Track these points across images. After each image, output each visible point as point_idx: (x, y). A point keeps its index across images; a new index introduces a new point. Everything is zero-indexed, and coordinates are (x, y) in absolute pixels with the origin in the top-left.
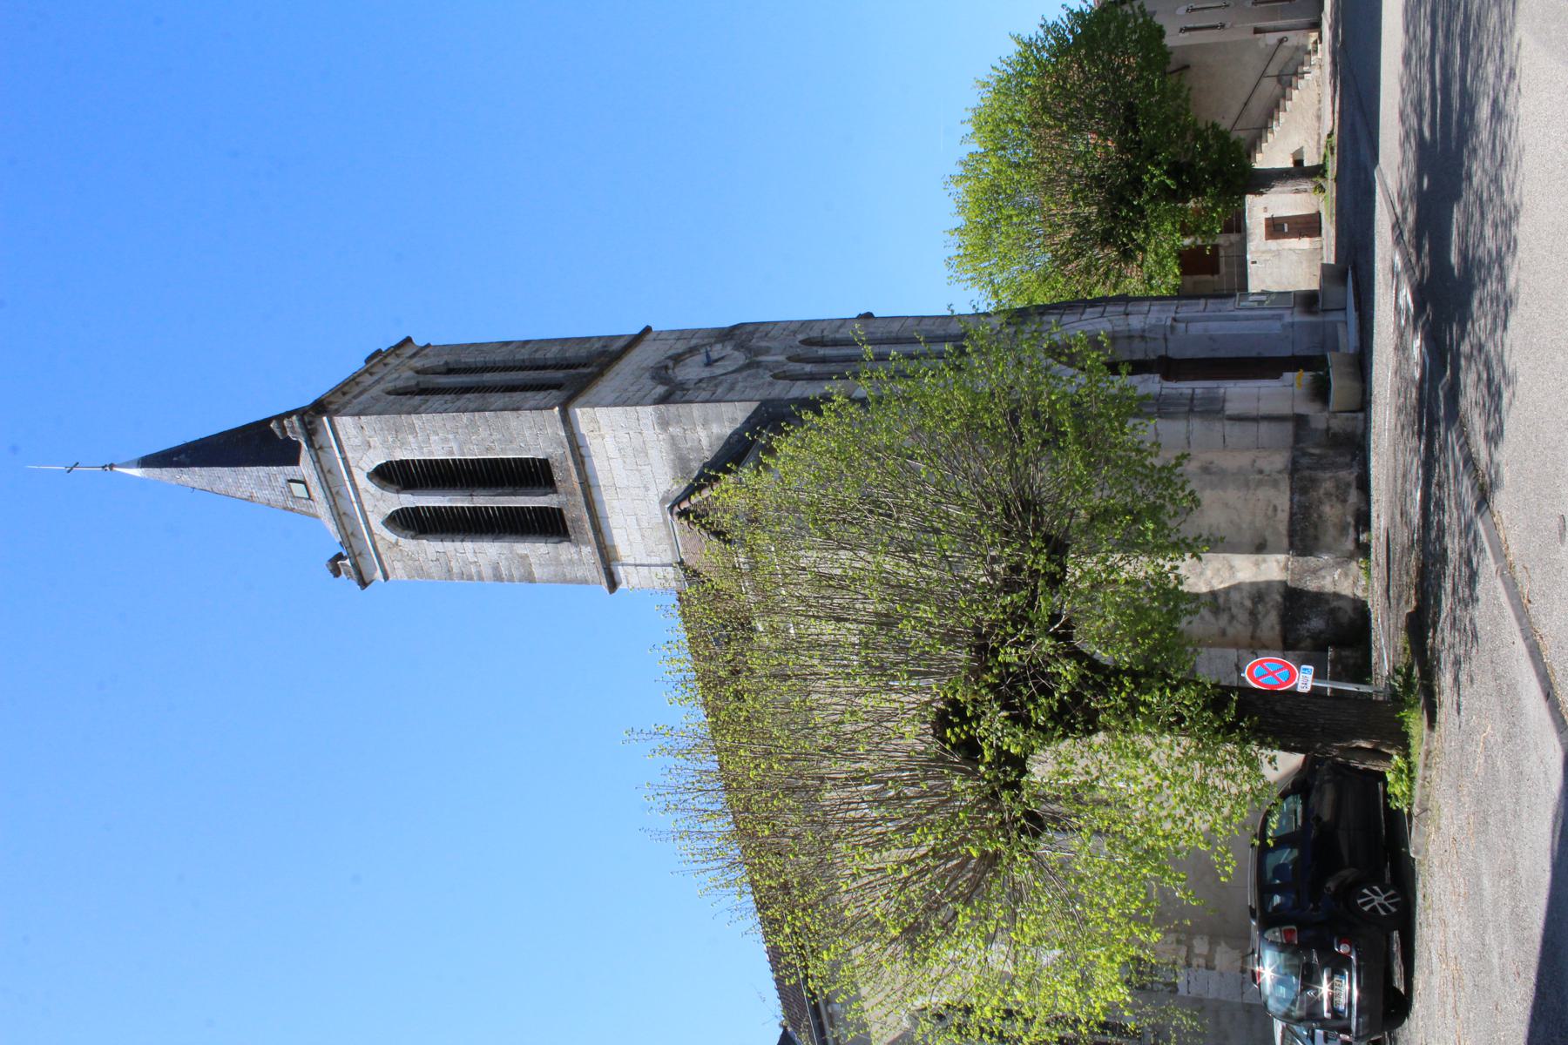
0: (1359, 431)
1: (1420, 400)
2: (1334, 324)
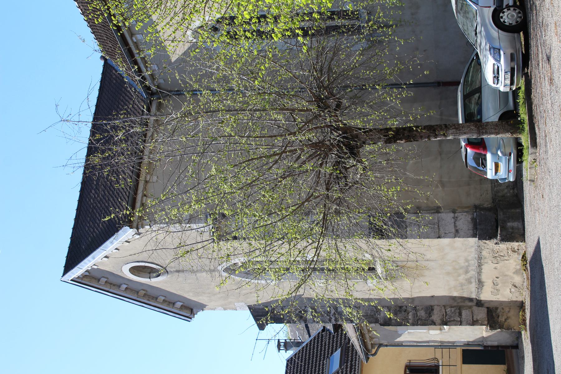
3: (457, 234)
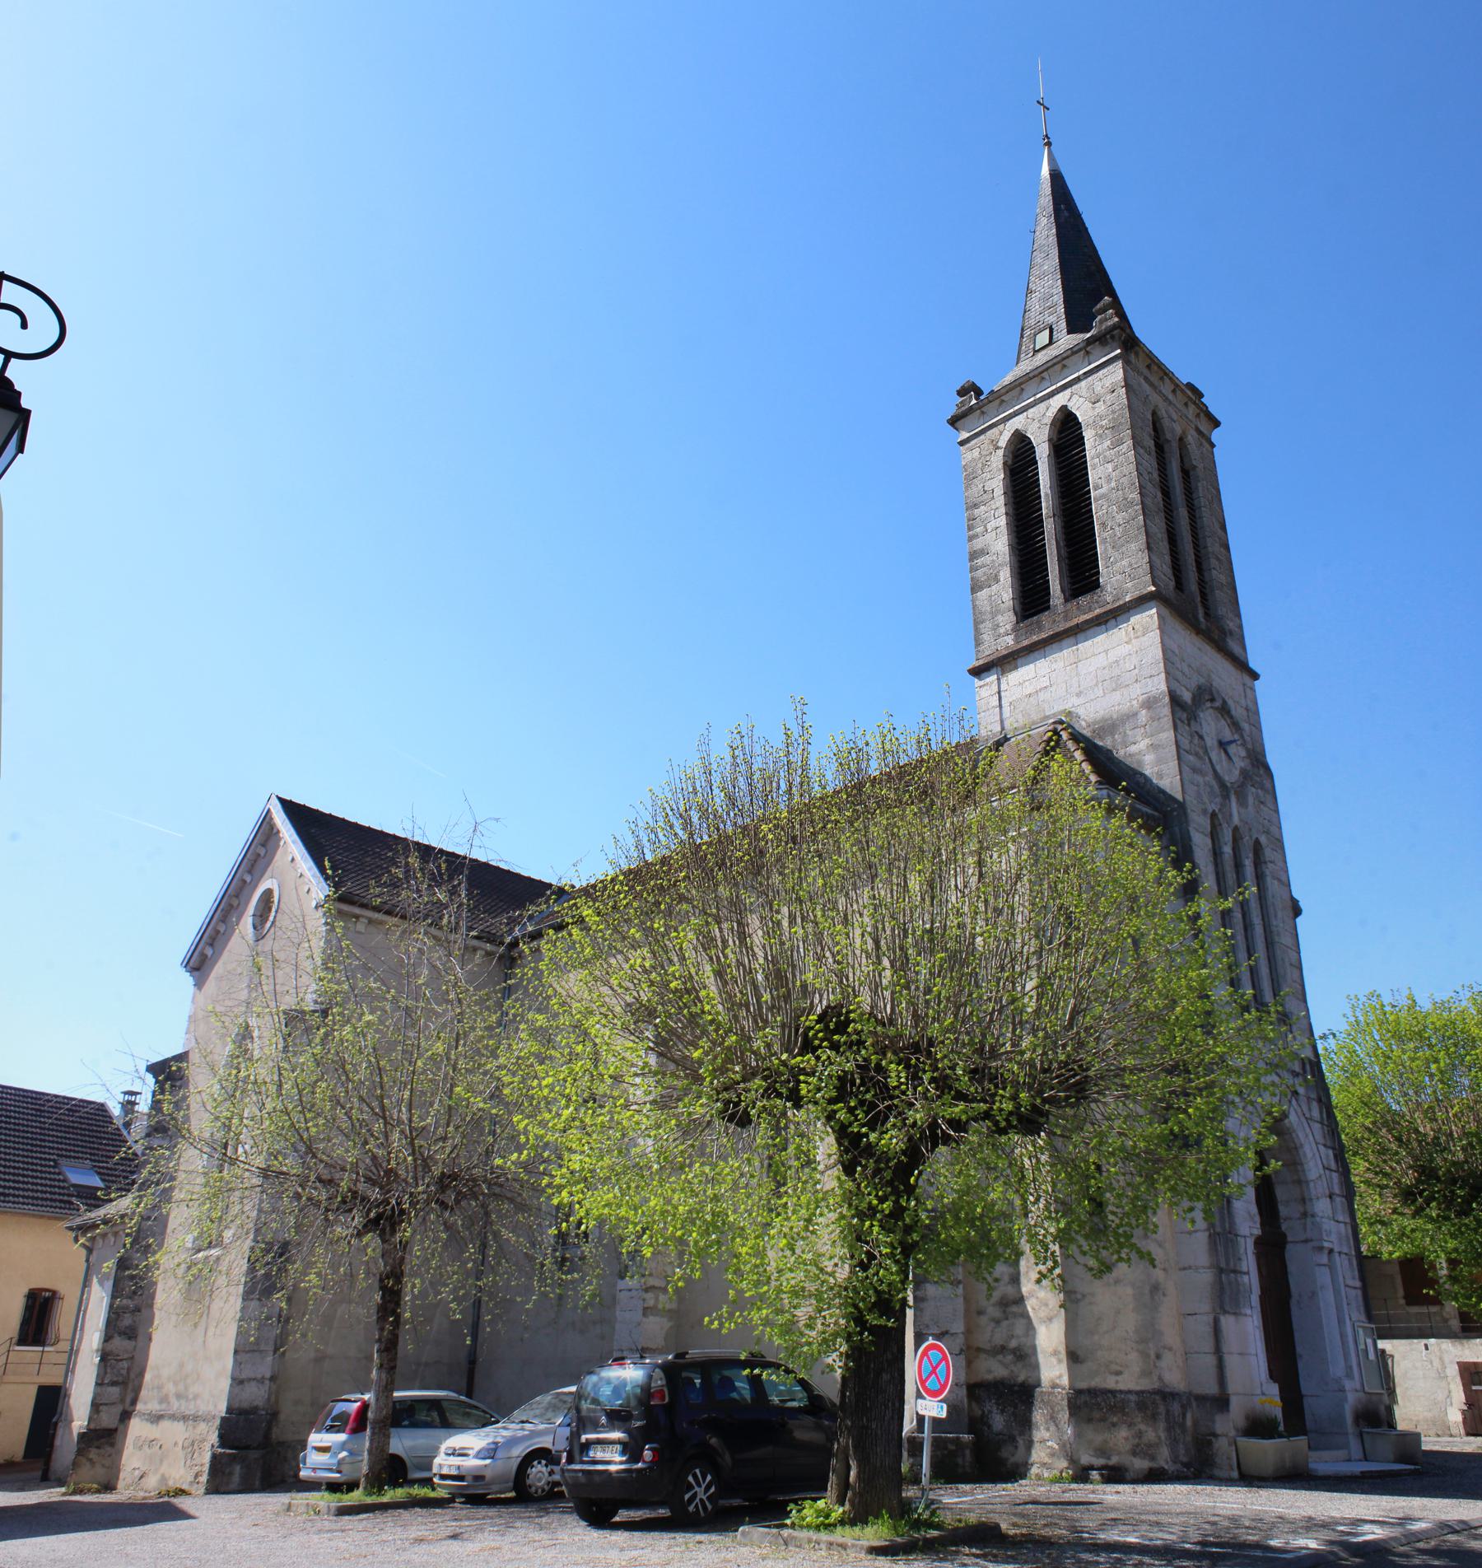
0: (1217, 1472)
1: (1244, 1545)
2: (1346, 1446)
3: (237, 1381)
